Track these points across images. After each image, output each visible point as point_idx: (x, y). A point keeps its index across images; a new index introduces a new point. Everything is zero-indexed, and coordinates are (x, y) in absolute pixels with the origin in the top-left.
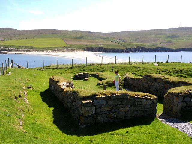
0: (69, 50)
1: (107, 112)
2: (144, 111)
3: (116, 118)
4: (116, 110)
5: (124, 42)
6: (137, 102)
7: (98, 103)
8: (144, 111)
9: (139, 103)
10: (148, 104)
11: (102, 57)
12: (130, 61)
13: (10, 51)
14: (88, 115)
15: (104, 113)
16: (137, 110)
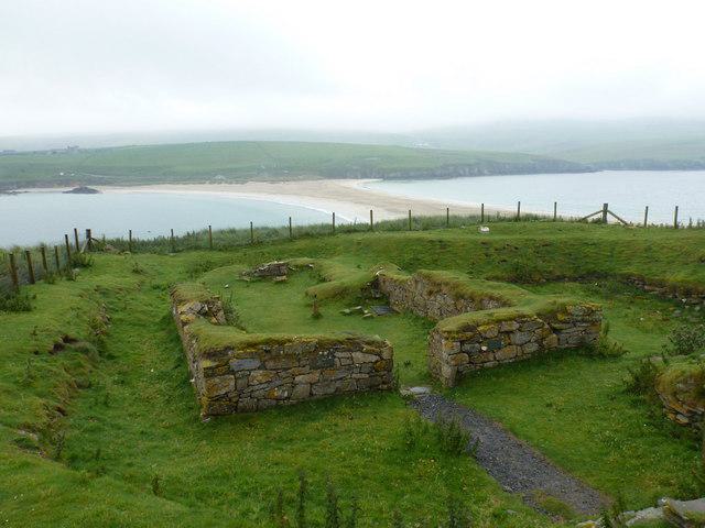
1: (266, 385)
3: (288, 398)
9: (344, 362)
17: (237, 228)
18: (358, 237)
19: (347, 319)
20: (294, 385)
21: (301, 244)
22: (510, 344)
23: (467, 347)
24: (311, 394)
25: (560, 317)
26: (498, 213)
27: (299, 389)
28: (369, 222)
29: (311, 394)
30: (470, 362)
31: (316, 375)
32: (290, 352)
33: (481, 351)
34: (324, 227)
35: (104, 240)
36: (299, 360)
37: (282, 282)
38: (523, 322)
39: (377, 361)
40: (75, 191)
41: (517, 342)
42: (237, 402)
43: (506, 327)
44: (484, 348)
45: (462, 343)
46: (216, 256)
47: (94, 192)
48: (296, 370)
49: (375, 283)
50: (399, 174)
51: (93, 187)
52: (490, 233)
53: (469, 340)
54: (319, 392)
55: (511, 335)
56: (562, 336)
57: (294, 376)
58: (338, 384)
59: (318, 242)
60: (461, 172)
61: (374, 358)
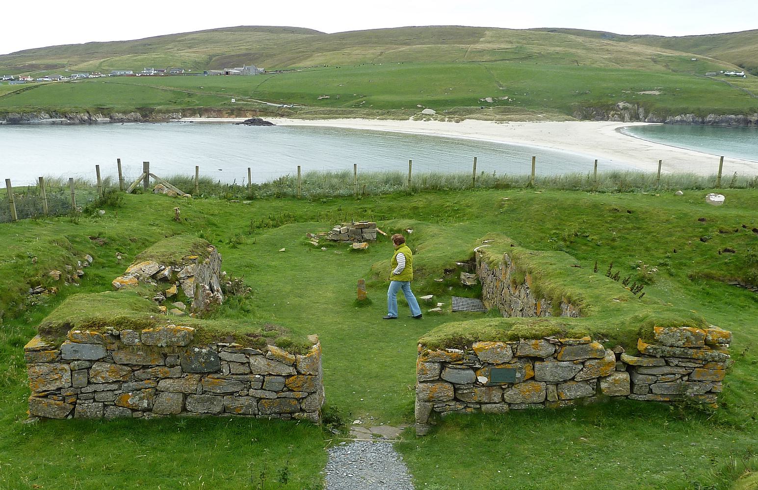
1: (115, 386)
2: (261, 399)
3: (149, 410)
14: (45, 389)
15: (101, 387)
16: (232, 394)
18: (505, 196)
20: (157, 392)
21: (419, 201)
22: (533, 378)
24: (184, 409)
25: (642, 345)
27: (164, 398)
29: (184, 409)
30: (456, 399)
32: (150, 342)
34: (462, 180)
35: (735, 177)
36: (165, 356)
37: (359, 251)
39: (289, 376)
40: (246, 123)
41: (549, 378)
42: (74, 404)
43: (529, 348)
44: (483, 380)
45: (443, 365)
46: (301, 209)
48: (161, 371)
49: (471, 264)
51: (269, 119)
52: (725, 205)
54: (197, 409)
55: (538, 364)
56: (639, 379)
57: (158, 380)
58: (227, 401)
59: (449, 201)
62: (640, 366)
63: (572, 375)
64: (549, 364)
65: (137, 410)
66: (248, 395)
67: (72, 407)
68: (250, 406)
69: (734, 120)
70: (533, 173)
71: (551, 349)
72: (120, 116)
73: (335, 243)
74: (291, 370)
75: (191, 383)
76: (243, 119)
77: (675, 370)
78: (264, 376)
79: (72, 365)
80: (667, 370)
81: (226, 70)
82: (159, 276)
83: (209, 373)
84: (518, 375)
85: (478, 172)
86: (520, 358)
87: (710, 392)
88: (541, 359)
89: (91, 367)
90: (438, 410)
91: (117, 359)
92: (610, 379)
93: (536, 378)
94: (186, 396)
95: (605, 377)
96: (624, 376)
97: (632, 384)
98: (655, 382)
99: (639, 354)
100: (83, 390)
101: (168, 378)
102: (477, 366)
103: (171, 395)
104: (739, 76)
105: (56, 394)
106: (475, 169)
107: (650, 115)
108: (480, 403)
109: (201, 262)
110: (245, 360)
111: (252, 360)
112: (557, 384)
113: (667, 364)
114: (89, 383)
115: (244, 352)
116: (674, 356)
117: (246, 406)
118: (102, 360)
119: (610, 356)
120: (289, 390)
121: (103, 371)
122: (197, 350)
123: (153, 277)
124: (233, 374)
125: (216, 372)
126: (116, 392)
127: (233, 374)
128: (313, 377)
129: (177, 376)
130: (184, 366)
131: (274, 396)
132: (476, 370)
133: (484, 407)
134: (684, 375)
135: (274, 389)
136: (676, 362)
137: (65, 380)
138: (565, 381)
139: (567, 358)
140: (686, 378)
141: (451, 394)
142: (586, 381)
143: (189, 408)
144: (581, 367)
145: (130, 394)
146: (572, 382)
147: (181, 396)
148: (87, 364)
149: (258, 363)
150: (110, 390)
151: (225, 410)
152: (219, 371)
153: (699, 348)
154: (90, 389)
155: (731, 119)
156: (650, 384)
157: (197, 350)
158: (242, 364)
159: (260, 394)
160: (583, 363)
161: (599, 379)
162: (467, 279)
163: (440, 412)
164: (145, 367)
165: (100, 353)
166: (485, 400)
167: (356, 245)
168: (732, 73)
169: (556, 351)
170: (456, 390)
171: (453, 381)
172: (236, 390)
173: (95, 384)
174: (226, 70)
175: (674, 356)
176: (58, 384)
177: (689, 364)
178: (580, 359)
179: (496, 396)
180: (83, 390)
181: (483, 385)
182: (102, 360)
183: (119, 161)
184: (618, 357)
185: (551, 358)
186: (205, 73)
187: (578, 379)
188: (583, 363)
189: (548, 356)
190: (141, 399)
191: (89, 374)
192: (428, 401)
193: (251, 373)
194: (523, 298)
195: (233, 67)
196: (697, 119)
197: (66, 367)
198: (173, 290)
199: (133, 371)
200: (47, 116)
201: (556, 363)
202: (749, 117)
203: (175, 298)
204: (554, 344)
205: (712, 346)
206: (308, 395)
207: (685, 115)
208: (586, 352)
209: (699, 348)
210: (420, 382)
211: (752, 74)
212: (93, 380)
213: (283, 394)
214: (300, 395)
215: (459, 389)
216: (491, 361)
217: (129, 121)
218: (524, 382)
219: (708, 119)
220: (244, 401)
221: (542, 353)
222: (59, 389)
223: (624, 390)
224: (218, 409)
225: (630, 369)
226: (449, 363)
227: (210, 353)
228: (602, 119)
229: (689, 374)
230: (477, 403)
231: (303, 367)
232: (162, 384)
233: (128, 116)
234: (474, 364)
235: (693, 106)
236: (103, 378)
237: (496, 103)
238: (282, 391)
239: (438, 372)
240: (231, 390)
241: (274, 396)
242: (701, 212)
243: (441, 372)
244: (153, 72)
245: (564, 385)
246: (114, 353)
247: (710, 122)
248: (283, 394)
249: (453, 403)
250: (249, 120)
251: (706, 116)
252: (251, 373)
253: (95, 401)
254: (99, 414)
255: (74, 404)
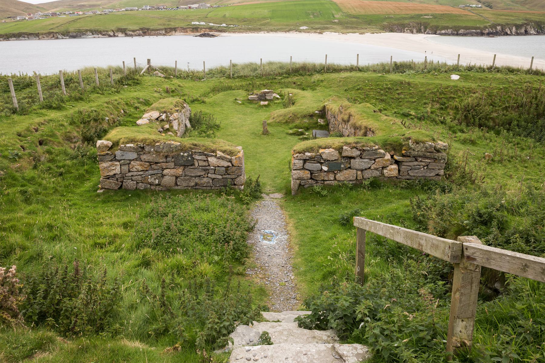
0: (347, 28)
1: (141, 173)
2: (214, 179)
3: (159, 185)
4: (156, 172)
5: (491, 7)
6: (198, 160)
7: (122, 155)
8: (213, 179)
9: (202, 163)
10: (223, 167)
11: (533, 58)
12: (137, 64)
13: (224, 32)
14: (108, 174)
15: (135, 173)
16: (199, 176)
17: (212, 68)
19: (290, 137)
20: (163, 176)
22: (350, 168)
23: (308, 165)
24: (176, 184)
26: (315, 66)
27: (166, 179)
28: (174, 67)
29: (176, 184)
30: (311, 178)
31: (180, 171)
33: (321, 170)
38: (364, 150)
39: (228, 167)
40: (201, 36)
44: (325, 168)
45: (305, 161)
47: (213, 36)
48: (164, 165)
49: (323, 113)
50: (450, 31)
53: (311, 159)
55: (352, 160)
57: (163, 170)
58: (197, 180)
60: (509, 32)
61: (226, 164)
62: (403, 162)
63: (369, 166)
64: (358, 160)
65: (153, 185)
66: (207, 177)
67: (121, 184)
68: (209, 182)
69: (475, 33)
70: (358, 64)
71: (358, 153)
72: (131, 33)
73: (251, 101)
74: (230, 164)
75: (180, 171)
76: (199, 34)
77: (420, 163)
78: (215, 167)
79: (121, 162)
80: (416, 163)
81: (189, 6)
82: (160, 119)
83: (188, 166)
84: (342, 166)
85: (327, 63)
86: (344, 157)
87: (438, 175)
88: (354, 158)
89: (130, 163)
90: (302, 184)
91: (142, 159)
92: (388, 168)
93: (351, 167)
94: (177, 178)
95: (386, 167)
96: (395, 166)
97: (399, 171)
98: (411, 170)
99: (403, 156)
100: (127, 175)
101: (168, 168)
102: (322, 161)
103: (170, 177)
104: (478, 7)
105: (113, 177)
106: (391, 59)
107: (428, 30)
108: (324, 180)
109: (181, 112)
110: (206, 159)
111: (209, 159)
112: (362, 171)
113: (416, 160)
114: (129, 171)
115: (205, 155)
116: (420, 157)
117: (207, 183)
118: (136, 159)
119: (388, 156)
120: (228, 174)
121: (137, 166)
122: (182, 154)
123: (157, 119)
124: (200, 166)
125: (191, 165)
126: (143, 176)
127: (200, 166)
128: (239, 168)
129: (173, 167)
130: (176, 162)
131: (220, 177)
132: (321, 163)
133: (326, 182)
134: (425, 166)
135: (220, 174)
136: (420, 159)
137: (117, 170)
138: (366, 169)
139: (367, 157)
140: (426, 168)
141: (309, 176)
142: (376, 169)
143: (178, 183)
144: (373, 162)
145: (149, 177)
146: (369, 170)
147: (174, 178)
148: (128, 162)
149: (212, 160)
150: (140, 175)
151: (196, 184)
152: (193, 165)
153: (432, 152)
154: (130, 174)
155: (473, 32)
156: (408, 171)
157: (182, 154)
158: (205, 161)
159: (213, 176)
160: (375, 160)
161: (383, 168)
162: (321, 121)
163: (304, 185)
164: (156, 163)
165: (135, 156)
166: (326, 179)
167: (262, 103)
168: (474, 6)
169: (361, 154)
170: (311, 174)
171: (310, 169)
172: (202, 174)
173: (132, 172)
174: (189, 6)
175: (420, 157)
176: (114, 172)
177: (426, 160)
178: (373, 157)
179: (331, 177)
180: (127, 175)
181: (325, 171)
182: (136, 159)
183: (135, 59)
184: (392, 157)
185: (359, 157)
186: (177, 7)
187: (372, 168)
188: (375, 160)
189: (357, 157)
190: (155, 179)
191: (129, 167)
192: (298, 179)
193: (209, 166)
194: (347, 129)
195: (193, 4)
196: (454, 32)
197: (118, 163)
198: (167, 126)
199: (151, 165)
200: (91, 34)
201: (361, 160)
202: (484, 31)
203: (168, 130)
204: (360, 150)
205: (438, 151)
206: (238, 177)
207: (447, 30)
208: (377, 154)
209: (432, 152)
210: (294, 170)
211: (485, 6)
212: (131, 170)
213: (225, 176)
214: (233, 177)
215: (313, 173)
216: (329, 159)
217: (136, 35)
218: (345, 169)
219: (460, 32)
220: (205, 180)
221: (354, 155)
222: (115, 175)
223: (395, 173)
224: (193, 184)
225: (397, 162)
226: (308, 160)
227: (188, 156)
228: (401, 32)
229: (427, 166)
230: (322, 180)
231: (234, 162)
232: (166, 172)
233: (136, 33)
234: (319, 159)
235: (450, 24)
236: (136, 169)
237: (340, 23)
238: (225, 175)
239: (302, 165)
240: (199, 174)
241: (220, 177)
242: (448, 83)
243: (304, 165)
244: (148, 8)
245: (366, 171)
246: (141, 156)
247: (461, 34)
248: (225, 176)
249: (310, 181)
250: (202, 34)
251: (459, 30)
252: (209, 166)
253: (132, 180)
254: (135, 187)
255: (122, 182)
